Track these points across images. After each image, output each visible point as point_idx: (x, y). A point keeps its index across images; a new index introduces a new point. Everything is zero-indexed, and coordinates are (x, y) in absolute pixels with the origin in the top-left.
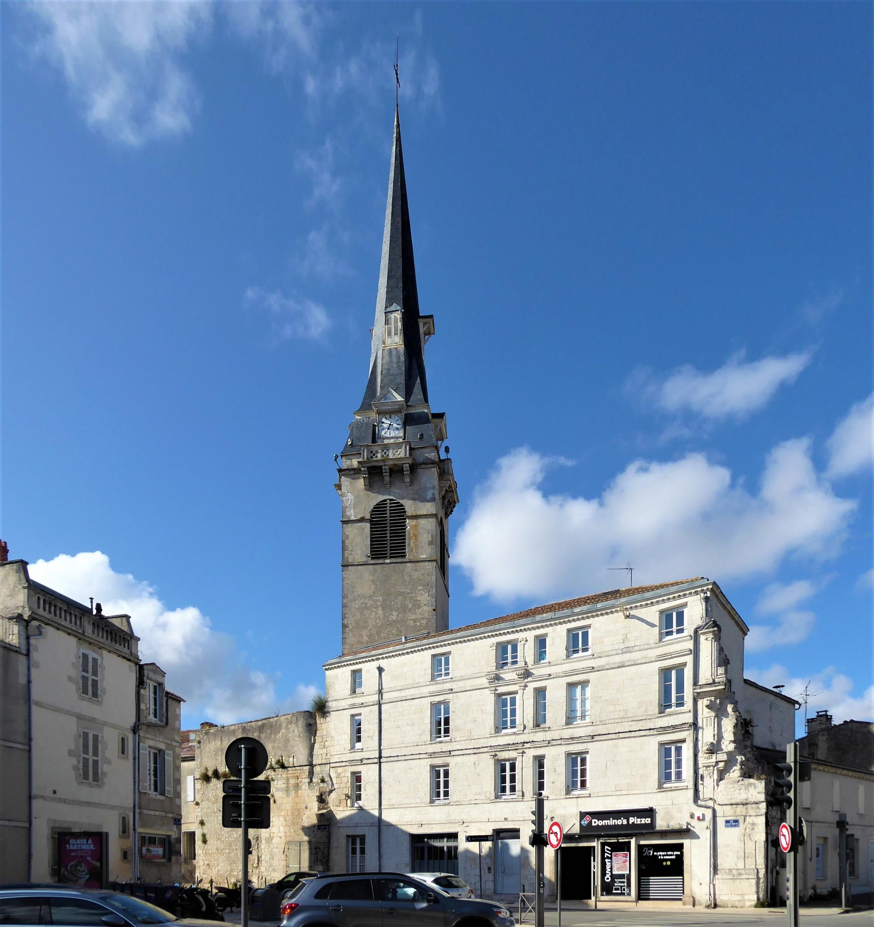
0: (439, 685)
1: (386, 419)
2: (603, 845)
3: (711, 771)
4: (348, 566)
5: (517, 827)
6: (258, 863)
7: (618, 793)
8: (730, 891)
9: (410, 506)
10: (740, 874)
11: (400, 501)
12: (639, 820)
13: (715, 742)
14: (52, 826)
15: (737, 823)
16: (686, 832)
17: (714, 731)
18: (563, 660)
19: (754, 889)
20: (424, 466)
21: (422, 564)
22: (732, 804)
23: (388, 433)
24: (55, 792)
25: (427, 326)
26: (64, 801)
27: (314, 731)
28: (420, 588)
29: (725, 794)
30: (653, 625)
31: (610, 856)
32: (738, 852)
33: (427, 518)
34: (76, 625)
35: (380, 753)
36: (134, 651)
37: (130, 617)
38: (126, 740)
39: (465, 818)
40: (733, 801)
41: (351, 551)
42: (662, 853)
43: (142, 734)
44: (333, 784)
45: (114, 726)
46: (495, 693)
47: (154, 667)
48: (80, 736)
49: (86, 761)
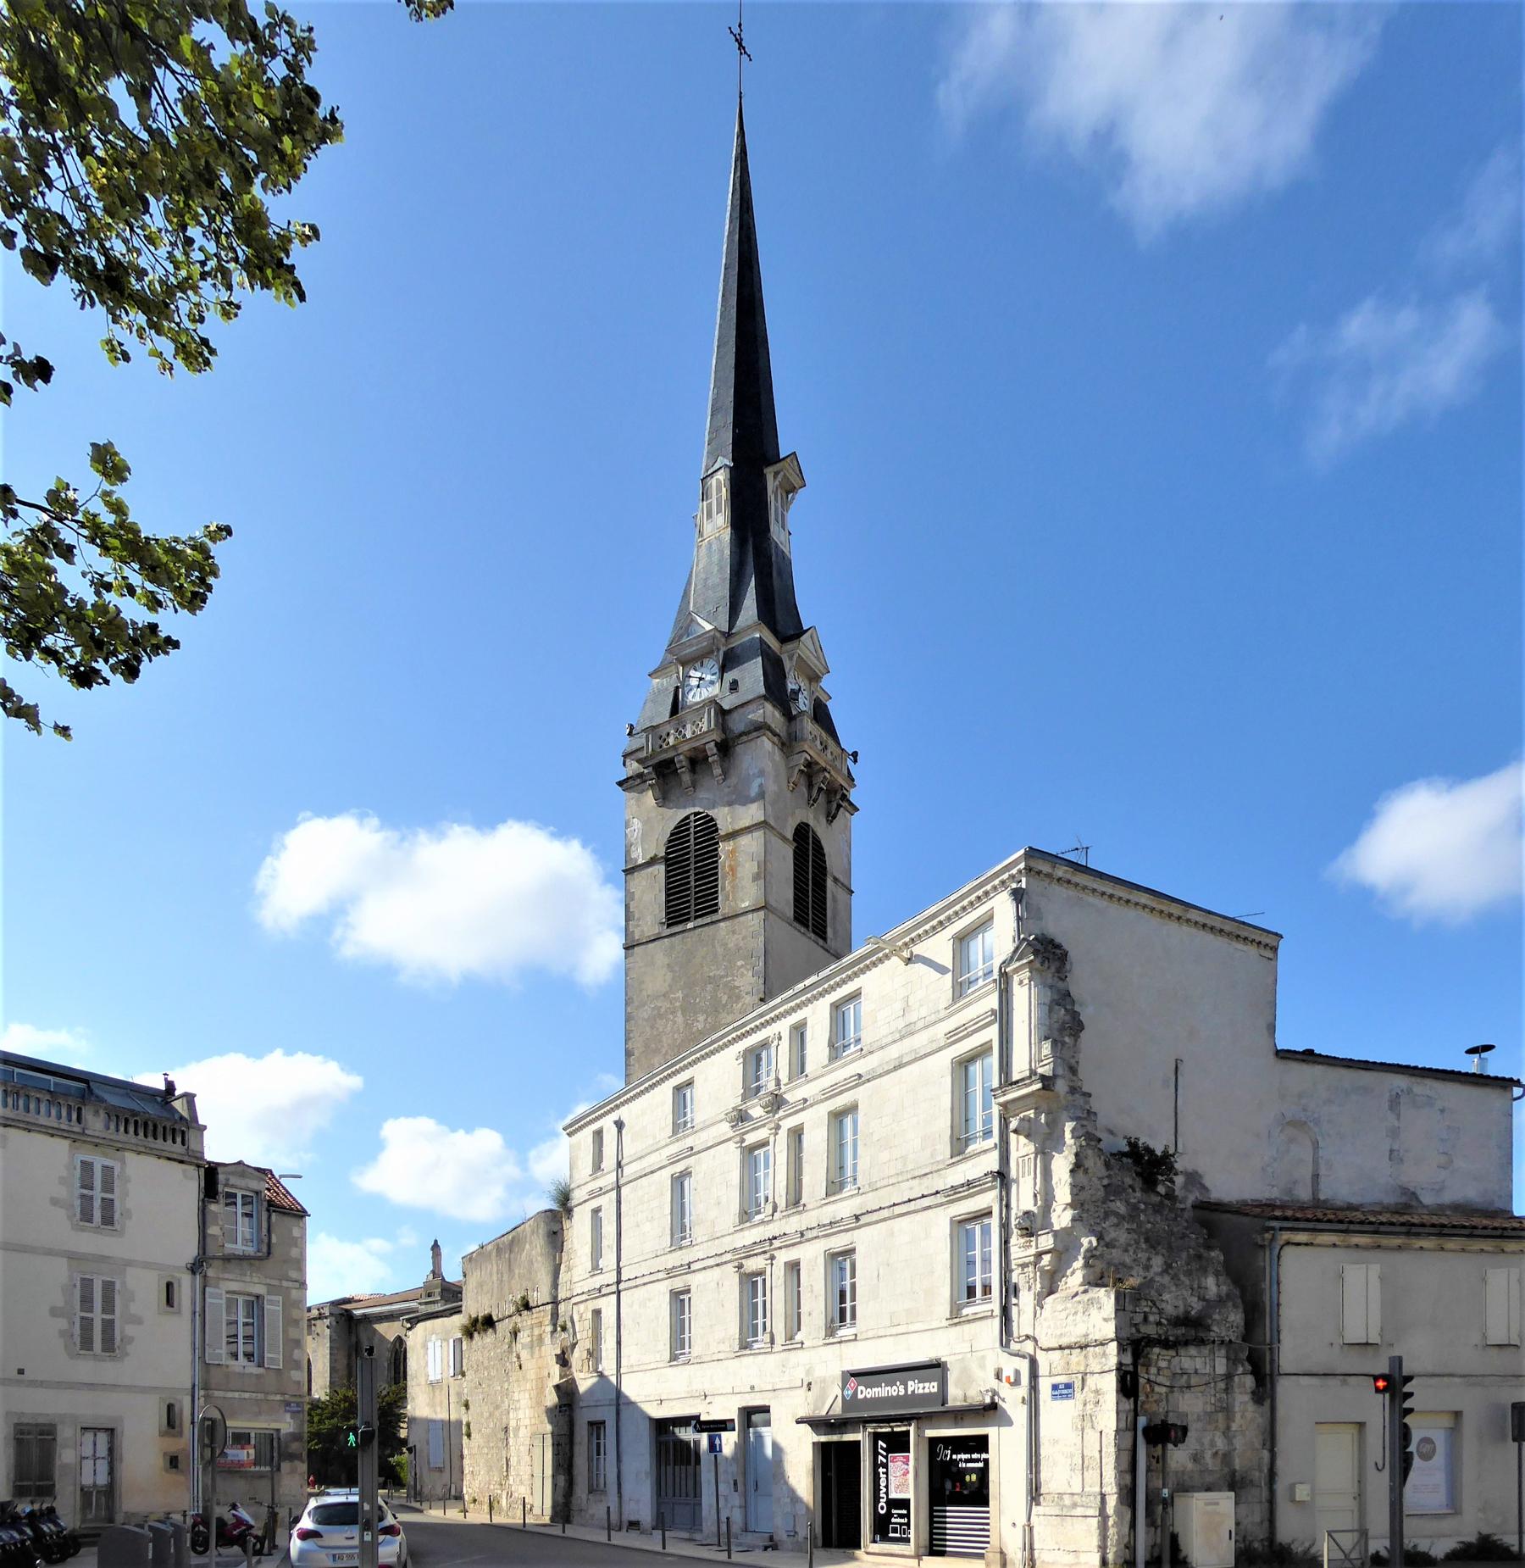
0: (680, 1142)
1: (696, 670)
2: (876, 1437)
3: (1032, 1275)
4: (633, 946)
5: (766, 1403)
6: (507, 1471)
7: (894, 1331)
8: (1057, 1543)
9: (725, 818)
10: (1075, 1505)
11: (710, 813)
12: (921, 1385)
13: (1035, 1209)
14: (16, 1421)
15: (1070, 1391)
16: (990, 1411)
17: (1035, 1184)
18: (823, 1067)
19: (1095, 1541)
20: (745, 738)
21: (742, 919)
22: (1061, 1348)
23: (698, 694)
24: (21, 1372)
25: (780, 477)
26: (41, 1384)
27: (560, 1244)
28: (739, 963)
29: (1052, 1326)
30: (942, 970)
31: (884, 1461)
32: (1072, 1456)
33: (751, 832)
34: (70, 1120)
35: (619, 1272)
36: (193, 1146)
37: (194, 1095)
38: (176, 1286)
39: (708, 1389)
40: (1064, 1341)
41: (639, 919)
42: (964, 1456)
43: (211, 1273)
44: (575, 1333)
45: (147, 1265)
46: (741, 1147)
47: (240, 1168)
48: (75, 1286)
49: (87, 1325)
